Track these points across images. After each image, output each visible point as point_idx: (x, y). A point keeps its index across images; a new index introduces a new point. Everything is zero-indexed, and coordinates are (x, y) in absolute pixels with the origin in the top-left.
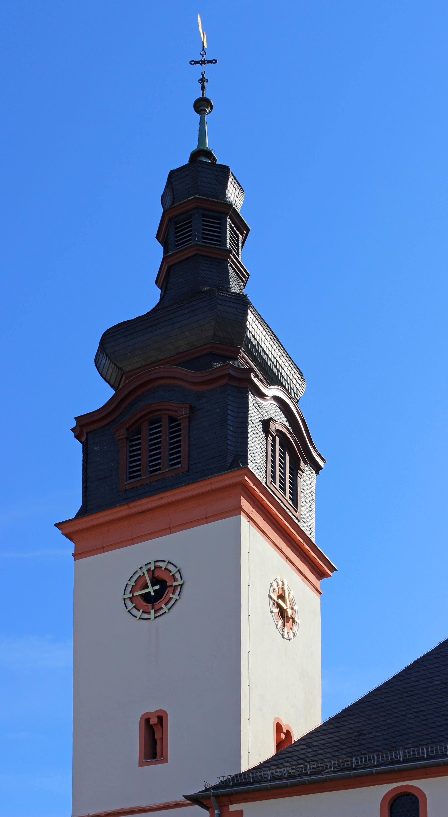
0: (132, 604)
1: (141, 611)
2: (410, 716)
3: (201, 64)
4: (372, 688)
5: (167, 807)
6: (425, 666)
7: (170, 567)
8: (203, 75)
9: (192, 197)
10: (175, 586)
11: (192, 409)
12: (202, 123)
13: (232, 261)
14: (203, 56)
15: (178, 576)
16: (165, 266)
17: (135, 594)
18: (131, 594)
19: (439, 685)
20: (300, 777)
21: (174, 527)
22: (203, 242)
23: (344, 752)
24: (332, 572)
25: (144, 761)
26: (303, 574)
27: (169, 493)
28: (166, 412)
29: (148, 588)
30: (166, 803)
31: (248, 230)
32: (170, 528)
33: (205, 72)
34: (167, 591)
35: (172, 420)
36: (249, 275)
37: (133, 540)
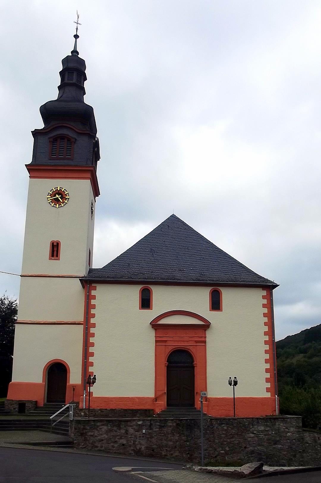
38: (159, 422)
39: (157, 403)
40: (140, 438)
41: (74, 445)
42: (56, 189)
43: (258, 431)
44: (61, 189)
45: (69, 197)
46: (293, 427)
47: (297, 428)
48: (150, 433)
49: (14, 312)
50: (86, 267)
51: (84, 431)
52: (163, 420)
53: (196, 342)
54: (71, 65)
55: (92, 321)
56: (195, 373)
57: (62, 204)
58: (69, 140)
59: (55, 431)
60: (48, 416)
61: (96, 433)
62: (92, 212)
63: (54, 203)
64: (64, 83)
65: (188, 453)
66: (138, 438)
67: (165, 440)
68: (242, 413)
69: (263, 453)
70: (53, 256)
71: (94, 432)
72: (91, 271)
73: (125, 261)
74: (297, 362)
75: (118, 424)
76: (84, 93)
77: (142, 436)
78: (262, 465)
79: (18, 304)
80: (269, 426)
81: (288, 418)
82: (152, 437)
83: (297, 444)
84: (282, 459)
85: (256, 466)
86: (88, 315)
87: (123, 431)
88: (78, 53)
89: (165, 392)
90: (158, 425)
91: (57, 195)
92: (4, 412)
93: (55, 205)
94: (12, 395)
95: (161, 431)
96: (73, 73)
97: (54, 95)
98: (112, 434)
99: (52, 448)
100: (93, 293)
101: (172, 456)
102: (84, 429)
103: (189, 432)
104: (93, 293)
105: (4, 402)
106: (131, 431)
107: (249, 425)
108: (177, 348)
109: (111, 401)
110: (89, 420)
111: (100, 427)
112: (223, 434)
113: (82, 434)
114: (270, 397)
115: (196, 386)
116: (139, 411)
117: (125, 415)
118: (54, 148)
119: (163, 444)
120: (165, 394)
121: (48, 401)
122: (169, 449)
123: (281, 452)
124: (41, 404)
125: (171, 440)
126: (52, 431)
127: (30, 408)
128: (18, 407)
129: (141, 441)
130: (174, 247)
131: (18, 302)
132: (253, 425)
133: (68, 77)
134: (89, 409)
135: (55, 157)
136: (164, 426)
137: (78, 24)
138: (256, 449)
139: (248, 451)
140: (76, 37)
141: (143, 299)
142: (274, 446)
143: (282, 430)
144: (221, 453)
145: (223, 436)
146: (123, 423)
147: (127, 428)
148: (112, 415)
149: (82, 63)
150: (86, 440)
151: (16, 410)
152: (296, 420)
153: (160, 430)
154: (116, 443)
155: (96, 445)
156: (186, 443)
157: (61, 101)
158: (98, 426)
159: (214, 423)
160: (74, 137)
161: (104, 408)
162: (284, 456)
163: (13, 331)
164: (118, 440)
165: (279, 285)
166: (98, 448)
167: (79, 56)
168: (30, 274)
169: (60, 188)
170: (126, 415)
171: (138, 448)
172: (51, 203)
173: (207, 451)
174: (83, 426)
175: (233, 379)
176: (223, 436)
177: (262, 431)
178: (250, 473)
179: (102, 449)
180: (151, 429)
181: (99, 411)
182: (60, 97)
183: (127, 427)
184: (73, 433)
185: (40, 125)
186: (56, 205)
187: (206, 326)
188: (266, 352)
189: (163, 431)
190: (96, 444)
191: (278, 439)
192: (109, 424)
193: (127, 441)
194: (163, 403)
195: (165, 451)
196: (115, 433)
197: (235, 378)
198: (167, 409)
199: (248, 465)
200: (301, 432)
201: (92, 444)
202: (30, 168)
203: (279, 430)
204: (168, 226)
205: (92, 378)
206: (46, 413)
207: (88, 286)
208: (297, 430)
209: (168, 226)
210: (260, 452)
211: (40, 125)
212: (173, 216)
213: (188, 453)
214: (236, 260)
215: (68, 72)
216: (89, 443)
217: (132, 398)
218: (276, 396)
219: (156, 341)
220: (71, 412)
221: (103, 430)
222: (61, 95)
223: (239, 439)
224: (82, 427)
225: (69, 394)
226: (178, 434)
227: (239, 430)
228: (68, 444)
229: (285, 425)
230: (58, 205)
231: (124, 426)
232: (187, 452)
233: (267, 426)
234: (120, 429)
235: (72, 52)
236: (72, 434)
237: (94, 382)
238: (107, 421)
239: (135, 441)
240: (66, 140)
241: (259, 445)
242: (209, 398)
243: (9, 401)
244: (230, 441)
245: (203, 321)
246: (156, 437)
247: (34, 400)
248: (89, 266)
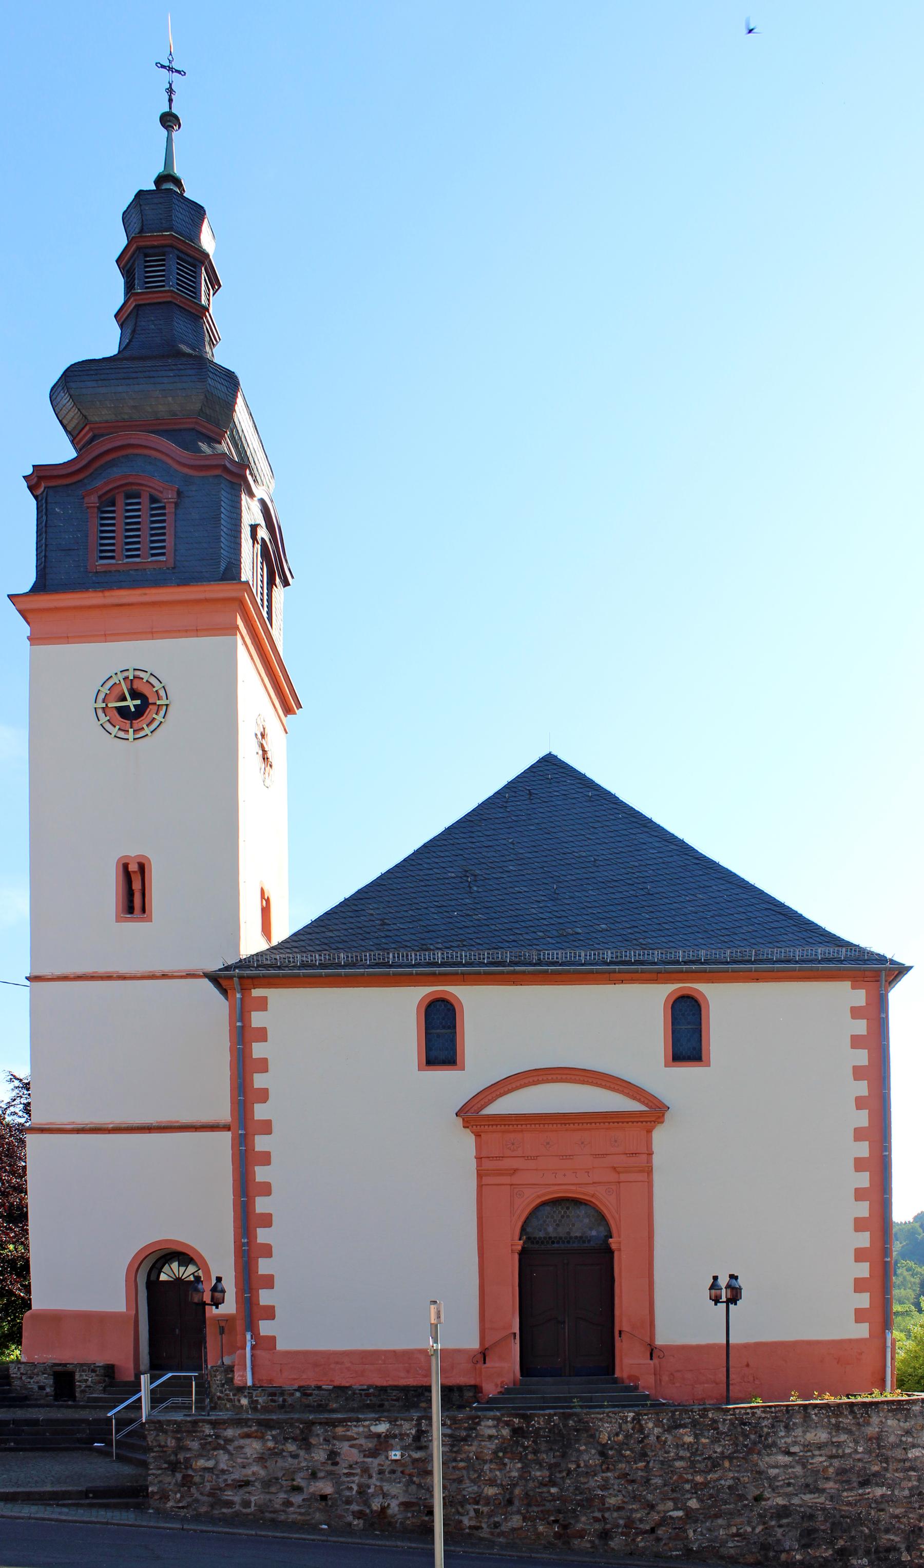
0: (106, 716)
1: (118, 727)
2: (433, 910)
3: (169, 70)
4: (384, 870)
5: (152, 977)
6: (435, 852)
7: (153, 681)
8: (171, 85)
9: (168, 233)
10: (159, 705)
11: (179, 493)
12: (169, 140)
13: (208, 321)
14: (170, 62)
15: (162, 693)
16: (132, 303)
17: (110, 705)
18: (105, 704)
19: (454, 878)
20: (332, 968)
21: (157, 632)
22: (178, 289)
23: (371, 943)
24: (298, 709)
25: (122, 915)
26: (276, 710)
27: (154, 591)
28: (147, 489)
29: (126, 700)
30: (150, 972)
31: (220, 286)
32: (152, 633)
33: (172, 82)
34: (149, 710)
35: (153, 500)
36: (220, 339)
37: (106, 637)
43: (807, 1447)
51: (181, 1457)
61: (223, 1460)
65: (555, 1521)
67: (473, 1481)
70: (130, 909)
84: (887, 1531)
87: (320, 1455)
89: (515, 1334)
100: (257, 1019)
101: (498, 1530)
102: (181, 1448)
106: (349, 1453)
107: (773, 1426)
109: (337, 1363)
115: (617, 1312)
117: (381, 1406)
119: (465, 1493)
122: (485, 1509)
123: (882, 1510)
125: (492, 1483)
127: (90, 1387)
128: (51, 1382)
129: (386, 1487)
130: (545, 859)
136: (469, 1436)
138: (796, 1501)
139: (765, 1510)
142: (860, 1491)
143: (892, 1439)
144: (671, 1517)
146: (318, 1430)
148: (338, 1405)
150: (187, 1481)
151: (48, 1390)
153: (455, 1449)
155: (226, 1497)
156: (545, 1489)
158: (228, 1441)
164: (303, 1484)
166: (232, 1508)
168: (58, 972)
170: (386, 1403)
173: (622, 1513)
174: (173, 1441)
175: (723, 1282)
180: (420, 1448)
181: (298, 1394)
183: (335, 1442)
189: (465, 1453)
190: (226, 1495)
191: (876, 1468)
193: (337, 1484)
195: (472, 1514)
197: (733, 1277)
201: (210, 1495)
203: (879, 1438)
204: (530, 794)
209: (530, 794)
210: (809, 1511)
213: (555, 1521)
231: (325, 1440)
232: (549, 1516)
241: (808, 1488)
242: (662, 1349)
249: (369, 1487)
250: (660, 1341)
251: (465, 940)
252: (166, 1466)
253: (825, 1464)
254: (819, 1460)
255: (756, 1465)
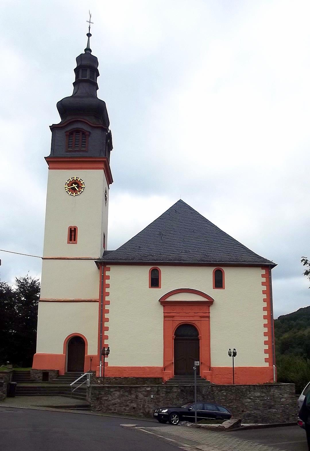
38: (166, 389)
39: (165, 372)
40: (148, 402)
41: (91, 408)
42: (73, 179)
43: (255, 397)
44: (78, 179)
45: (84, 186)
46: (287, 393)
47: (291, 394)
48: (157, 398)
49: (37, 290)
50: (101, 250)
51: (100, 396)
52: (168, 387)
53: (201, 317)
54: (84, 63)
55: (107, 299)
56: (200, 346)
57: (78, 192)
58: (83, 133)
59: (74, 396)
60: (69, 383)
61: (110, 398)
62: (106, 199)
63: (71, 192)
64: (79, 80)
66: (147, 402)
68: (241, 381)
69: (259, 416)
70: (71, 240)
71: (108, 396)
72: (106, 253)
73: (136, 244)
74: (308, 333)
75: (130, 390)
76: (97, 88)
77: (150, 400)
78: (240, 421)
79: (41, 283)
80: (265, 393)
81: (282, 385)
82: (159, 402)
83: (290, 408)
85: (235, 422)
86: (103, 293)
87: (133, 396)
88: (91, 51)
90: (164, 391)
91: (73, 185)
92: (30, 380)
93: (72, 193)
94: (37, 365)
95: (167, 396)
96: (87, 70)
97: (68, 91)
98: (124, 399)
99: (72, 411)
100: (107, 273)
102: (100, 394)
103: (192, 397)
104: (107, 273)
105: (29, 371)
106: (141, 396)
107: (246, 391)
108: (185, 322)
110: (103, 387)
111: (114, 393)
112: (223, 399)
113: (98, 399)
114: (268, 366)
116: (150, 379)
118: (70, 143)
120: (173, 364)
121: (68, 371)
124: (63, 373)
126: (72, 397)
128: (42, 375)
131: (40, 281)
132: (250, 392)
133: (82, 73)
134: (104, 378)
135: (72, 149)
137: (91, 23)
138: (253, 412)
139: (245, 415)
140: (89, 35)
141: (153, 278)
143: (277, 396)
145: (222, 401)
146: (134, 389)
147: (137, 393)
149: (95, 60)
150: (101, 403)
152: (289, 387)
153: (167, 395)
154: (127, 406)
157: (78, 97)
158: (112, 392)
159: (215, 390)
160: (88, 130)
161: (118, 376)
162: (278, 419)
163: (37, 307)
164: (129, 404)
165: (277, 265)
167: (92, 53)
168: (51, 257)
169: (77, 178)
171: (147, 411)
172: (68, 192)
175: (232, 351)
176: (222, 401)
177: (258, 397)
178: (229, 427)
179: (115, 412)
180: (158, 395)
181: (114, 379)
182: (75, 93)
183: (137, 393)
184: (90, 398)
185: (57, 120)
186: (73, 194)
187: (210, 302)
188: (265, 326)
191: (273, 404)
192: (121, 390)
193: (138, 404)
194: (170, 372)
196: (126, 397)
197: (235, 349)
198: (175, 377)
199: (228, 421)
200: (294, 398)
202: (49, 160)
203: (273, 396)
205: (106, 349)
206: (67, 381)
207: (103, 267)
208: (290, 396)
211: (57, 120)
212: (180, 201)
214: (238, 242)
215: (82, 70)
216: (104, 407)
217: (143, 367)
218: (274, 366)
219: (165, 317)
220: (88, 380)
221: (116, 395)
222: (75, 91)
223: (237, 403)
224: (98, 392)
225: (87, 364)
226: (183, 399)
227: (237, 396)
228: (86, 407)
229: (279, 391)
230: (74, 193)
233: (263, 392)
234: (131, 394)
235: (85, 50)
236: (89, 399)
237: (108, 354)
238: (120, 387)
239: (144, 405)
240: (81, 133)
241: (255, 409)
243: (34, 371)
244: (229, 405)
245: (207, 298)
246: (162, 402)
247: (56, 370)
248: (104, 248)
249: (145, 405)
250: (212, 366)
251: (161, 253)
252: (96, 399)
253: (260, 402)
254: (258, 401)
255: (242, 402)
